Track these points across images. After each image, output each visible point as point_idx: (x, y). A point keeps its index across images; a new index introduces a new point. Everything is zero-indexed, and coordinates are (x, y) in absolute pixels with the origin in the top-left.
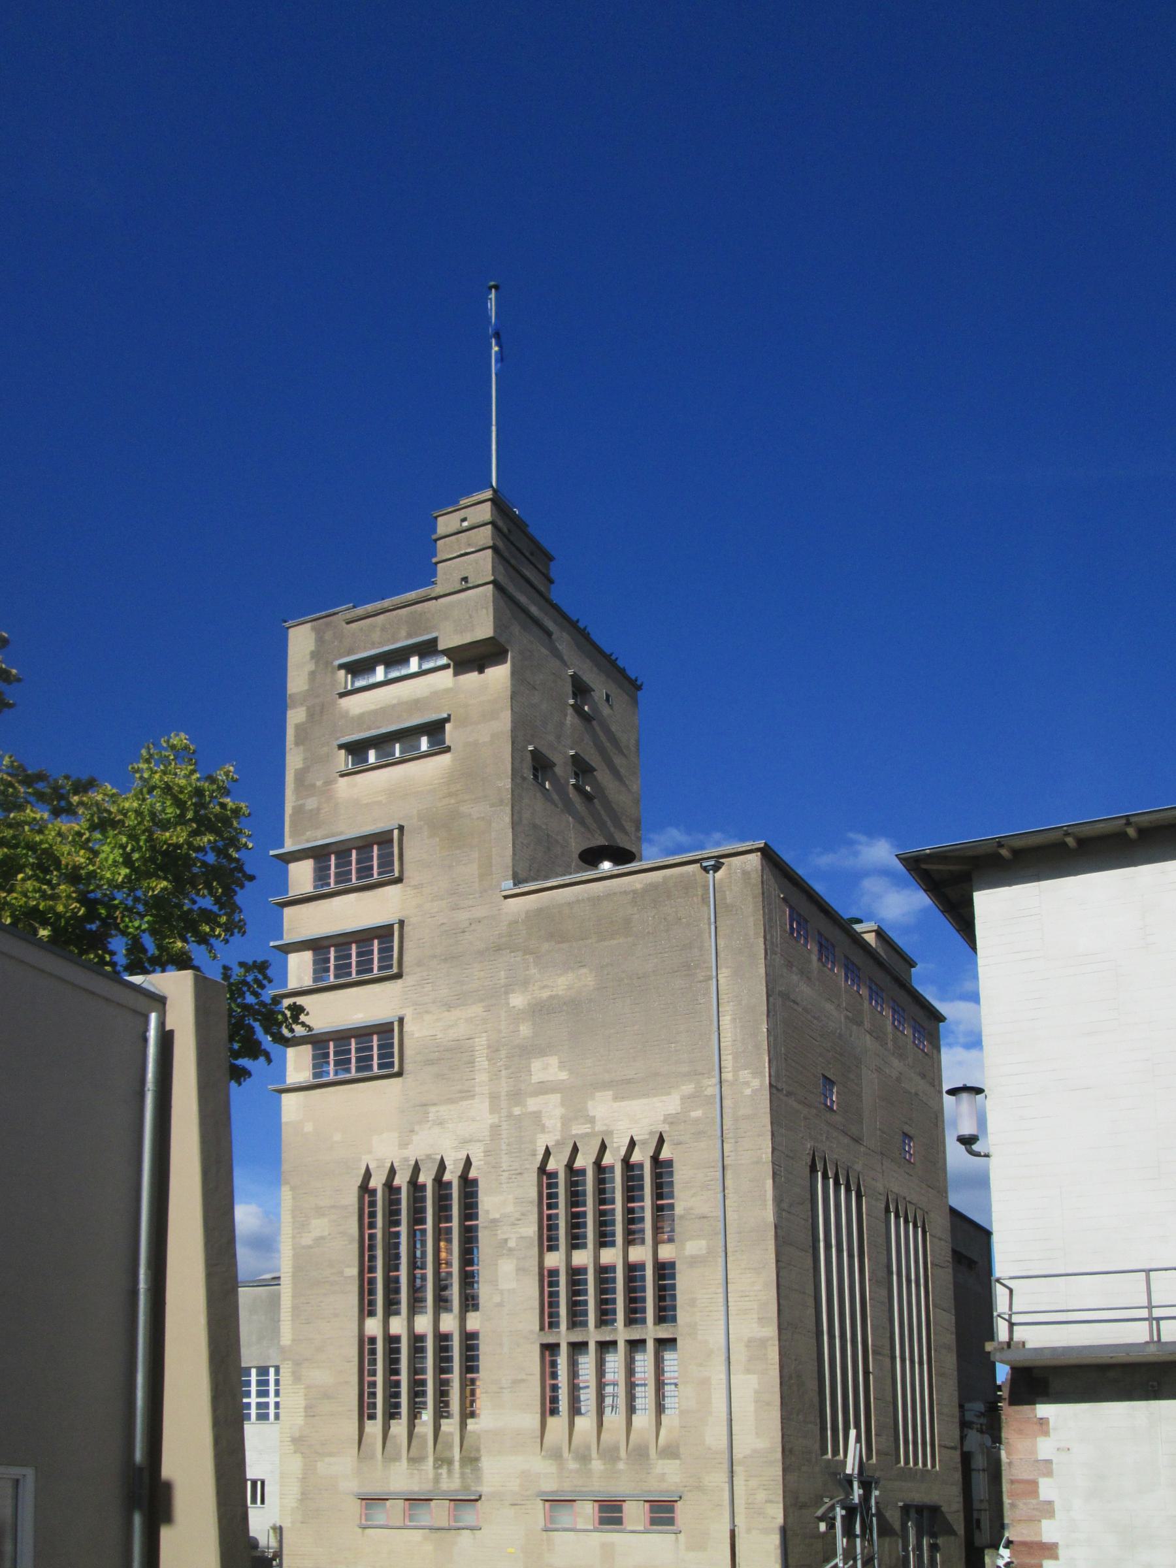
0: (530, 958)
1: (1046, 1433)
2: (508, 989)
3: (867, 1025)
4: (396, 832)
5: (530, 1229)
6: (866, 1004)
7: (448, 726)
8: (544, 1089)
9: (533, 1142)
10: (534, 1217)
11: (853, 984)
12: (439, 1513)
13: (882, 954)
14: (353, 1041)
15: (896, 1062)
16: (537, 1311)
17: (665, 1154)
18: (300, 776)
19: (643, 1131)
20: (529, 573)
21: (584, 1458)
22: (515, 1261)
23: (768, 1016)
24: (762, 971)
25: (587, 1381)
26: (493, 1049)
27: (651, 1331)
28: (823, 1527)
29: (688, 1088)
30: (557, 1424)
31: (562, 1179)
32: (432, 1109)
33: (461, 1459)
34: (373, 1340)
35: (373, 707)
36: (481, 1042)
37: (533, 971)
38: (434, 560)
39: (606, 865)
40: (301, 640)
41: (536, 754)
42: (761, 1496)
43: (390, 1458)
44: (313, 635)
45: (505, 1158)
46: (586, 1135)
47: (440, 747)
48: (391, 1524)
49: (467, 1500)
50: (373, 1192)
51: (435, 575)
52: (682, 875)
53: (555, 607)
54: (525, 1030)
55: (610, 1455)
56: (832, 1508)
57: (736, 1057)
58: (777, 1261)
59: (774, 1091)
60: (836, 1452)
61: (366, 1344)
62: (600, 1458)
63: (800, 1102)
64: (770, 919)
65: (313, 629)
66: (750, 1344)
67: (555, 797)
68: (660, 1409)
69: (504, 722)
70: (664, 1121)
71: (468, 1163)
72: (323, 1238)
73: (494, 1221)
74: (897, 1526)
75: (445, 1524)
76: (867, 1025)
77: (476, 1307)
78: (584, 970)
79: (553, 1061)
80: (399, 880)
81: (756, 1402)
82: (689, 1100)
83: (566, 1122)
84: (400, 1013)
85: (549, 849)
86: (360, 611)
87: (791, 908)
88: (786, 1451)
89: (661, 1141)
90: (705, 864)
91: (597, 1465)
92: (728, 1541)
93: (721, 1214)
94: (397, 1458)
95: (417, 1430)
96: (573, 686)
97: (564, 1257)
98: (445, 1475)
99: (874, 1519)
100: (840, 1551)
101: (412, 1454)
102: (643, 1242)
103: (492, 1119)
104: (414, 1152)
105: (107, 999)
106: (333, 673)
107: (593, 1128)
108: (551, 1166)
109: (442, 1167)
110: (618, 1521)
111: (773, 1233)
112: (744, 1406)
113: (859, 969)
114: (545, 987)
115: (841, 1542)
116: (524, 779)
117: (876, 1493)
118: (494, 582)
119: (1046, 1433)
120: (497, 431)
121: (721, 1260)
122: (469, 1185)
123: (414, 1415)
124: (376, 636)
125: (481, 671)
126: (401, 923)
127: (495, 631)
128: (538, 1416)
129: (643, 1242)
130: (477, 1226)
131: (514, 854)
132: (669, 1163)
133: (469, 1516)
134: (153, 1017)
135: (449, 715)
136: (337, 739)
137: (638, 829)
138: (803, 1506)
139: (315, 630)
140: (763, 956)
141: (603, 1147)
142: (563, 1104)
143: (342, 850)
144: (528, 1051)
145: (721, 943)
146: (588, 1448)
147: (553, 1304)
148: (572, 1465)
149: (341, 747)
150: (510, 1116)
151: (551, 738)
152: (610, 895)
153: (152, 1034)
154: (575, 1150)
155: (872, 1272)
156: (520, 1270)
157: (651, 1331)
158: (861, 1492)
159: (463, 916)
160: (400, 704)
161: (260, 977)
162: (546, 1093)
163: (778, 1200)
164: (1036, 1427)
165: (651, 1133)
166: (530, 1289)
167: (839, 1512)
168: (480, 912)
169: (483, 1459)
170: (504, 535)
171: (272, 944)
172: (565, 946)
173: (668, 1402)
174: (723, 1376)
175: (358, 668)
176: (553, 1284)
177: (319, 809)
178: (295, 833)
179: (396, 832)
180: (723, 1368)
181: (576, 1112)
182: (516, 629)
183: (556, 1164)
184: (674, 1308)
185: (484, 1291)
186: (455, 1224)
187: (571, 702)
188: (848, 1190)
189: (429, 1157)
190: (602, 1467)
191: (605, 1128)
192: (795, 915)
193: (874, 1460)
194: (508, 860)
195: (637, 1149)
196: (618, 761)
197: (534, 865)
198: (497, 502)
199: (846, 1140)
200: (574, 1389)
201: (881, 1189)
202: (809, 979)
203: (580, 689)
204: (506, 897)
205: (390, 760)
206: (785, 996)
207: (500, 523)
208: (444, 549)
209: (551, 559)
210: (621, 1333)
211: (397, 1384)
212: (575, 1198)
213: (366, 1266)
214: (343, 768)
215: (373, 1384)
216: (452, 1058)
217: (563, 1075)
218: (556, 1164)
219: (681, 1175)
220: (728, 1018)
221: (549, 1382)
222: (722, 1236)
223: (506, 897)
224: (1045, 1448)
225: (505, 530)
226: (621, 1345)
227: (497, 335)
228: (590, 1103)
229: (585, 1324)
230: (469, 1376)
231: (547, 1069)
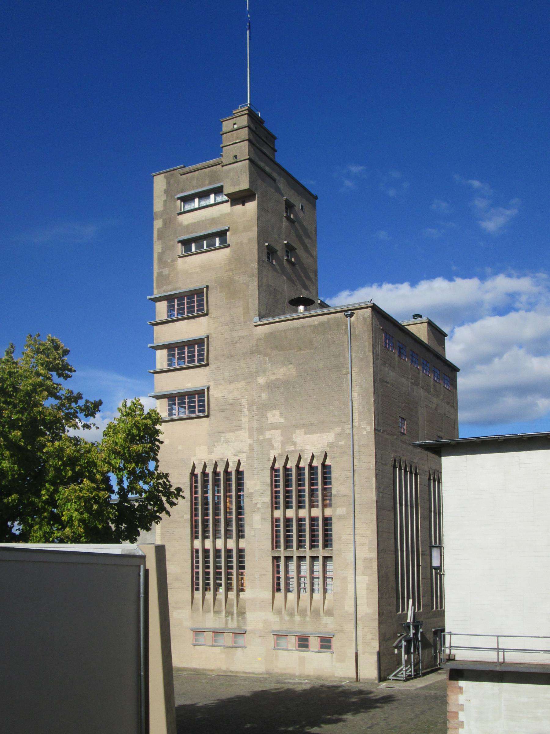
0: (267, 358)
1: (462, 693)
2: (257, 374)
3: (421, 384)
4: (205, 289)
7: (228, 233)
8: (274, 426)
9: (268, 454)
10: (269, 493)
11: (415, 365)
12: (227, 639)
14: (186, 397)
15: (435, 400)
16: (271, 540)
17: (327, 463)
18: (161, 256)
20: (265, 149)
21: (291, 615)
22: (260, 514)
23: (374, 394)
24: (372, 370)
25: (293, 575)
26: (251, 405)
27: (321, 552)
28: (396, 651)
29: (338, 429)
30: (280, 596)
31: (281, 473)
32: (223, 435)
33: (237, 613)
34: (197, 551)
35: (193, 221)
36: (245, 401)
37: (268, 365)
38: (221, 146)
39: (301, 308)
40: (159, 183)
41: (269, 247)
42: (369, 636)
43: (206, 611)
44: (165, 181)
45: (256, 461)
46: (293, 451)
47: (225, 244)
48: (206, 644)
49: (239, 633)
50: (196, 476)
51: (222, 152)
52: (336, 318)
53: (278, 165)
54: (265, 396)
55: (303, 613)
56: (401, 641)
57: (360, 414)
58: (377, 519)
60: (403, 610)
61: (194, 552)
62: (299, 615)
63: (388, 434)
64: (376, 342)
65: (165, 177)
66: (365, 559)
67: (278, 267)
68: (325, 590)
69: (254, 233)
70: (327, 446)
71: (239, 463)
73: (251, 494)
74: (431, 641)
75: (230, 645)
77: (243, 537)
78: (291, 366)
79: (277, 412)
80: (207, 314)
82: (339, 435)
83: (283, 444)
84: (208, 384)
85: (275, 296)
86: (187, 169)
87: (386, 333)
88: (380, 614)
89: (326, 456)
90: (346, 314)
91: (297, 618)
92: (355, 658)
93: (352, 494)
94: (208, 611)
95: (217, 597)
97: (282, 513)
98: (230, 621)
100: (404, 662)
101: (215, 609)
102: (317, 506)
105: (127, 565)
106: (175, 202)
107: (295, 448)
108: (276, 466)
109: (227, 465)
110: (306, 646)
111: (375, 505)
113: (417, 355)
114: (274, 374)
115: (404, 657)
116: (263, 261)
117: (421, 630)
118: (248, 127)
119: (462, 693)
120: (250, 71)
121: (352, 518)
122: (239, 473)
123: (216, 590)
124: (194, 183)
125: (243, 205)
126: (208, 337)
127: (250, 185)
129: (317, 506)
131: (259, 303)
132: (330, 467)
133: (241, 641)
134: (142, 566)
135: (229, 228)
136: (177, 237)
137: (316, 275)
138: (388, 639)
139: (166, 178)
140: (372, 362)
141: (300, 458)
142: (282, 435)
143: (180, 297)
144: (266, 407)
145: (353, 354)
146: (293, 609)
147: (278, 536)
148: (286, 618)
149: (179, 242)
150: (258, 440)
151: (276, 236)
152: (303, 327)
153: (142, 573)
154: (287, 459)
155: (421, 514)
156: (263, 519)
157: (321, 552)
158: (414, 632)
159: (236, 334)
160: (206, 220)
161: (165, 480)
162: (274, 429)
163: (378, 488)
164: (458, 690)
165: (321, 452)
166: (266, 530)
167: (404, 643)
168: (244, 333)
169: (247, 613)
171: (149, 346)
172: (282, 352)
173: (329, 587)
174: (353, 576)
177: (169, 274)
178: (158, 287)
179: (205, 289)
180: (353, 572)
181: (288, 440)
182: (259, 182)
183: (279, 465)
184: (331, 540)
185: (247, 529)
186: (233, 494)
187: (285, 214)
188: (411, 473)
189: (221, 459)
190: (300, 619)
191: (300, 448)
192: (388, 337)
193: (421, 610)
194: (256, 306)
195: (315, 459)
196: (306, 241)
197: (269, 310)
198: (251, 114)
200: (287, 579)
201: (427, 470)
202: (394, 368)
203: (289, 206)
204: (256, 326)
205: (202, 250)
206: (382, 380)
207: (252, 126)
208: (226, 139)
209: (275, 138)
211: (208, 573)
212: (287, 483)
215: (198, 573)
216: (232, 408)
217: (282, 420)
218: (279, 465)
219: (335, 474)
220: (356, 394)
221: (276, 575)
222: (352, 506)
223: (256, 326)
224: (461, 699)
225: (254, 129)
226: (308, 559)
227: (249, 28)
228: (294, 435)
229: (292, 547)
230: (240, 571)
231: (274, 417)
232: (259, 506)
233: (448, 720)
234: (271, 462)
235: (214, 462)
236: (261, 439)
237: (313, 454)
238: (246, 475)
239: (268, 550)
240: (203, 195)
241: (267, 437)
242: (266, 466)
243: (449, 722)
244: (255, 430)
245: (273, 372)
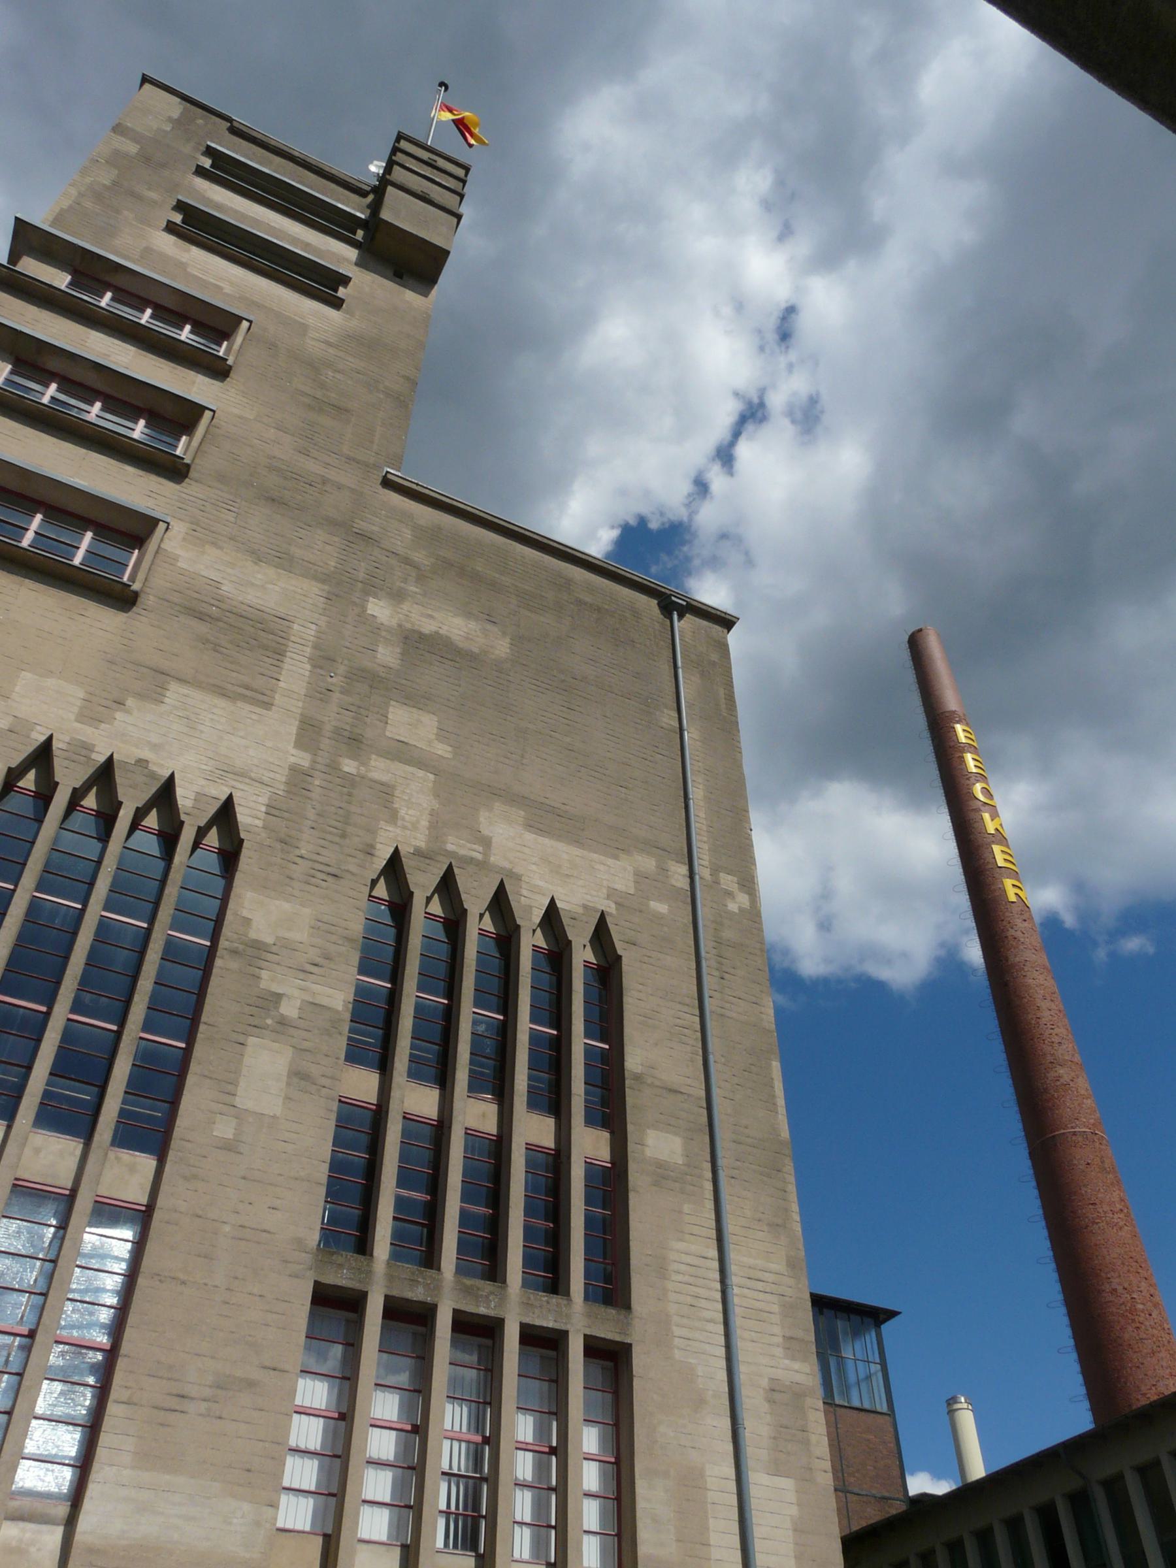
2: (371, 587)
8: (402, 753)
22: (289, 1052)
32: (174, 686)
166: (313, 1146)
217: (442, 750)
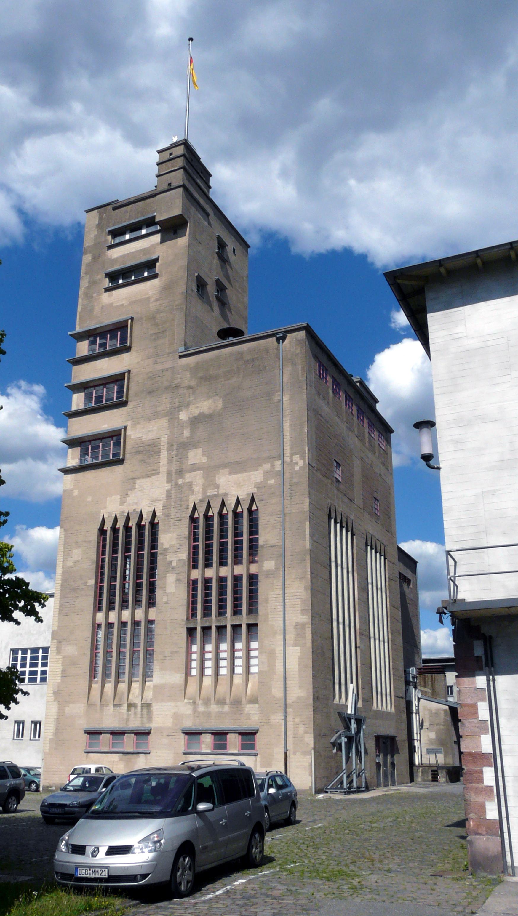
2: (179, 409)
5: (184, 555)
6: (355, 419)
8: (195, 468)
9: (188, 500)
10: (186, 547)
13: (205, 807)
15: (370, 455)
19: (244, 494)
22: (175, 575)
46: (215, 496)
59: (311, 467)
71: (154, 514)
72: (78, 561)
73: (166, 549)
75: (131, 750)
76: (356, 433)
78: (217, 398)
79: (199, 451)
81: (299, 665)
83: (205, 489)
84: (125, 424)
96: (218, 243)
98: (132, 716)
99: (344, 767)
103: (168, 486)
104: (126, 509)
107: (218, 491)
112: (293, 665)
114: (198, 407)
116: (192, 290)
117: (364, 727)
122: (154, 526)
123: (117, 682)
126: (129, 372)
128: (184, 675)
130: (157, 552)
150: (176, 484)
156: (178, 580)
157: (244, 619)
159: (160, 367)
167: (344, 740)
170: (189, 162)
174: (282, 648)
175: (115, 233)
176: (195, 589)
181: (210, 482)
188: (347, 531)
191: (224, 491)
192: (321, 364)
199: (346, 500)
203: (222, 245)
210: (229, 620)
213: (100, 579)
214: (107, 286)
216: (150, 450)
217: (204, 460)
232: (174, 564)
233: (460, 720)
234: (190, 510)
235: (126, 514)
236: (179, 483)
237: (238, 498)
238: (161, 527)
239: (182, 620)
240: (135, 227)
241: (187, 481)
242: (184, 515)
243: (463, 725)
244: (174, 474)
245: (197, 405)
